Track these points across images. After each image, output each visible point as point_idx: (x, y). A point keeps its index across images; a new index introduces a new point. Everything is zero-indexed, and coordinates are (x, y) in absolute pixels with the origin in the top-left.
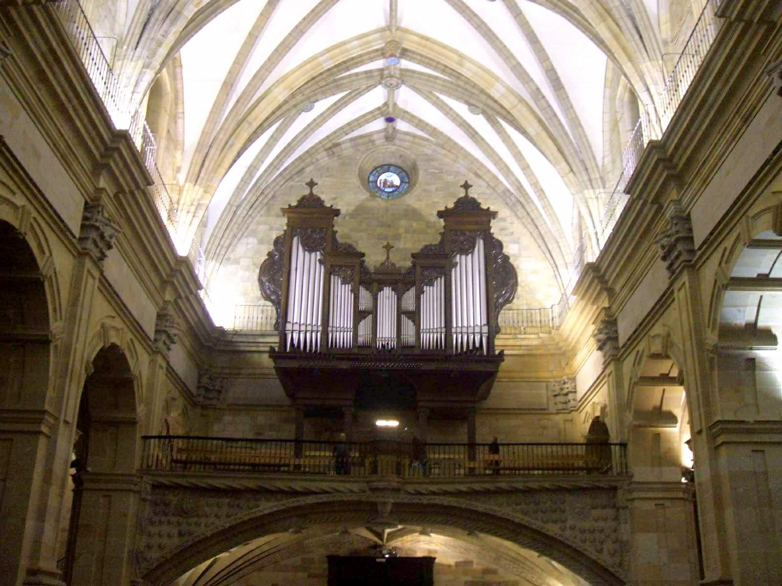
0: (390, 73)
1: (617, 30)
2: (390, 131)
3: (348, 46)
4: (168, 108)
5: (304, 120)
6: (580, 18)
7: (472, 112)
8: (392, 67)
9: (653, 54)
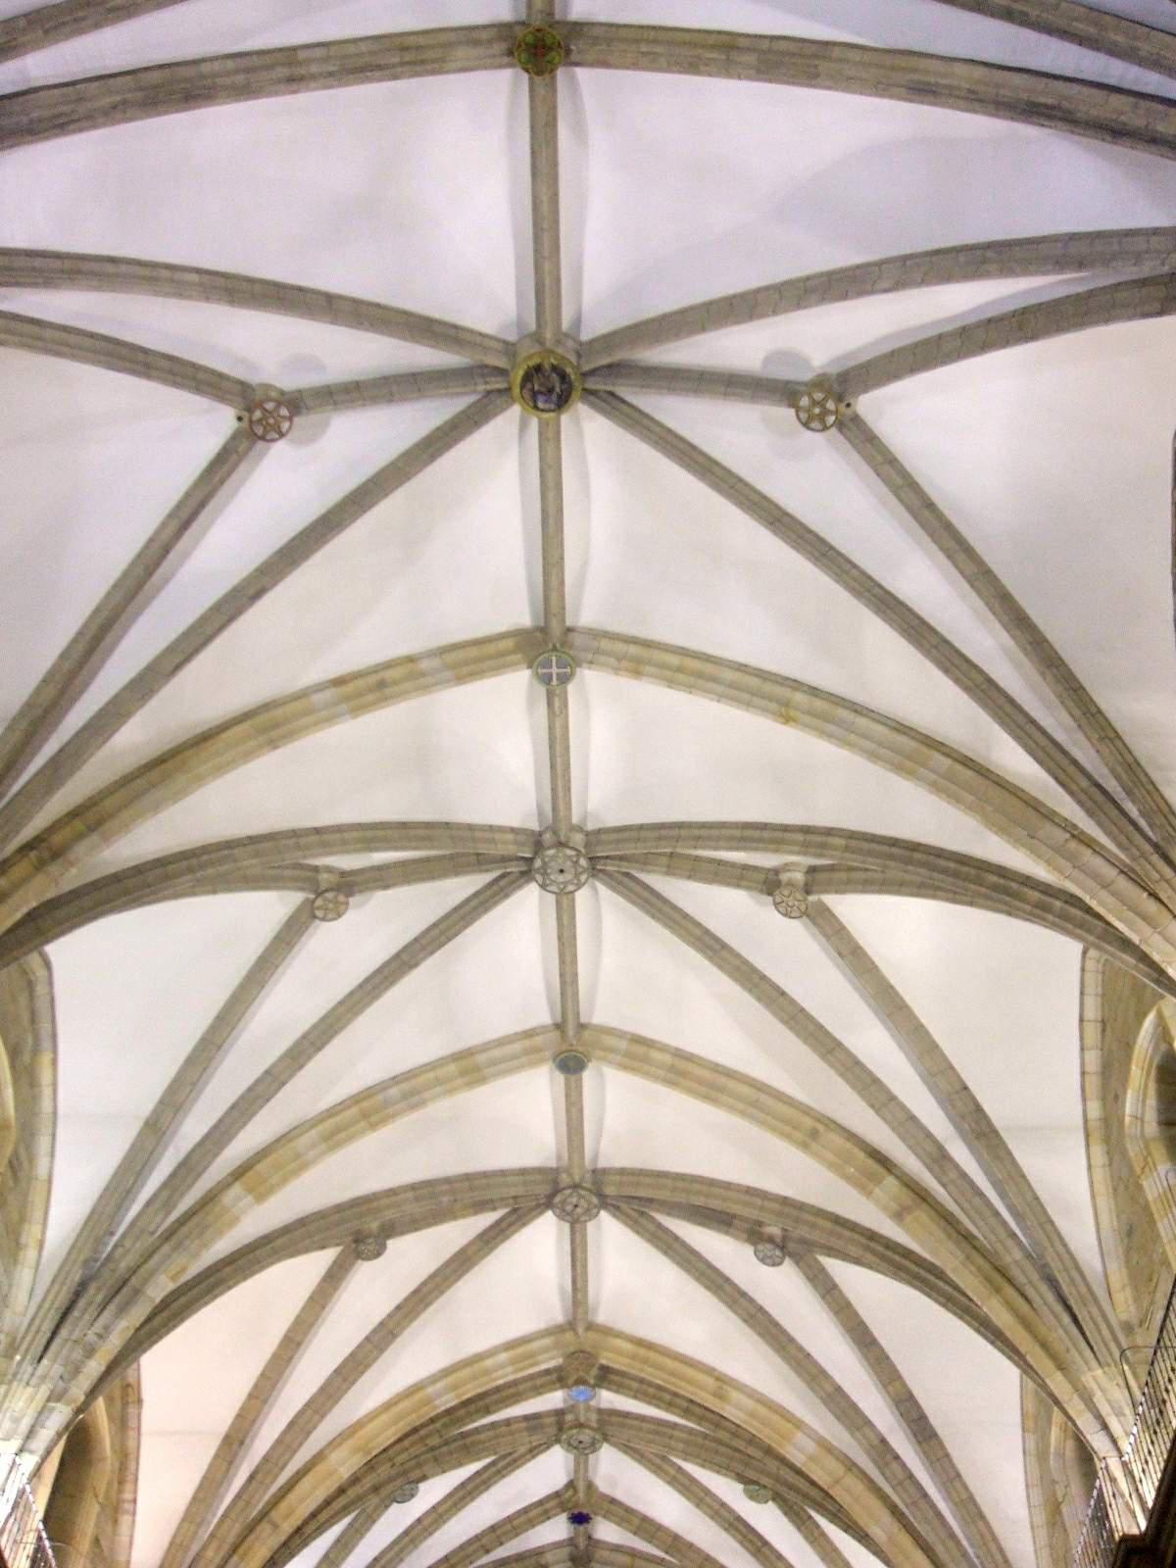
0: (577, 1419)
1: (1024, 1307)
2: (582, 1543)
3: (489, 1363)
4: (102, 1489)
5: (396, 1519)
6: (949, 1289)
7: (752, 1497)
8: (582, 1407)
9: (1104, 1350)
